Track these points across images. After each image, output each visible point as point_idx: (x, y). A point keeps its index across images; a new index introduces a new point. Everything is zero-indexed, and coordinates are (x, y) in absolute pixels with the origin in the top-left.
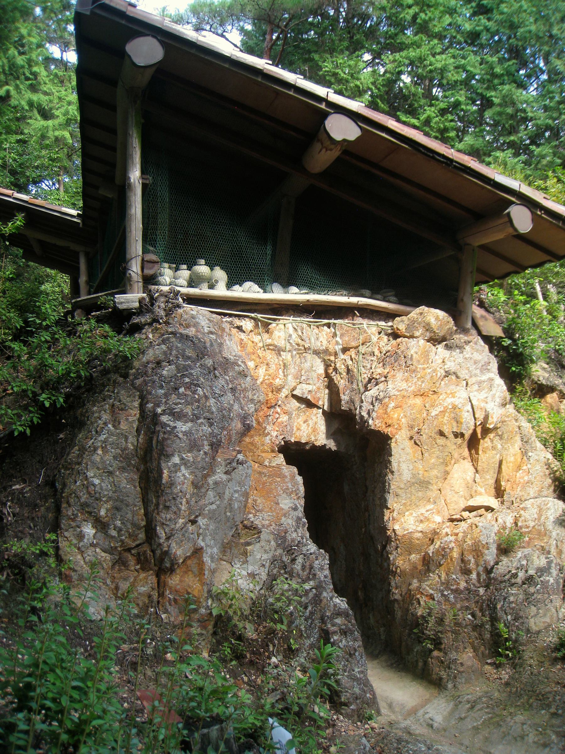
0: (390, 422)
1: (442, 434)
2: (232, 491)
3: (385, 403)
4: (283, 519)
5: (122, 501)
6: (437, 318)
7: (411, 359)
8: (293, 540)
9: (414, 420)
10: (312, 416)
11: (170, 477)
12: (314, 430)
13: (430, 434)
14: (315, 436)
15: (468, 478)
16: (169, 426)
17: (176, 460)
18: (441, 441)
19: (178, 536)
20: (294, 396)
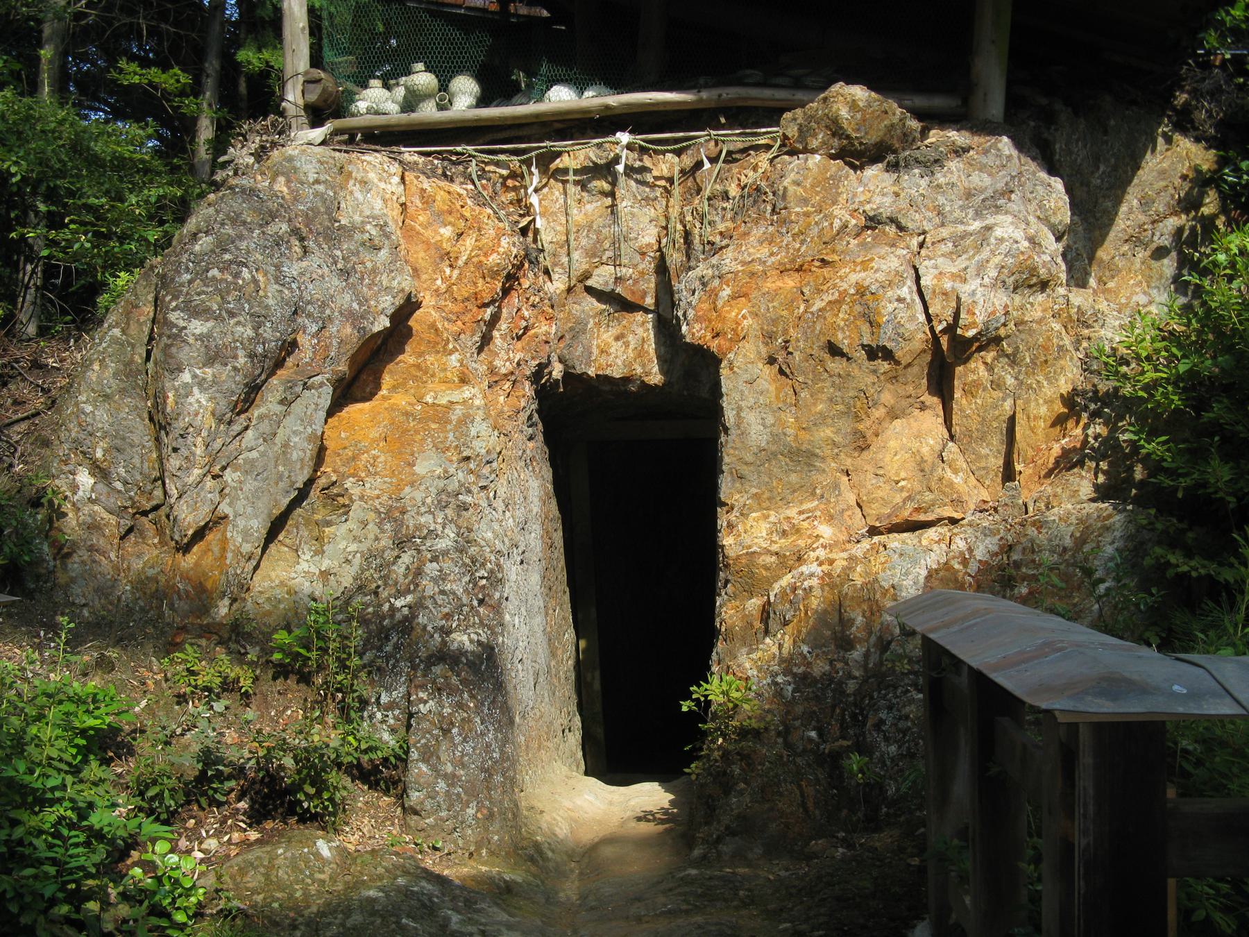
0: (719, 326)
1: (834, 350)
2: (288, 431)
3: (712, 290)
4: (407, 489)
5: (124, 439)
6: (853, 106)
7: (784, 197)
8: (418, 527)
9: (774, 322)
10: (634, 327)
11: (177, 403)
12: (640, 353)
13: (809, 351)
14: (643, 366)
15: (925, 450)
16: (176, 326)
17: (186, 377)
18: (836, 365)
19: (192, 493)
20: (590, 290)
